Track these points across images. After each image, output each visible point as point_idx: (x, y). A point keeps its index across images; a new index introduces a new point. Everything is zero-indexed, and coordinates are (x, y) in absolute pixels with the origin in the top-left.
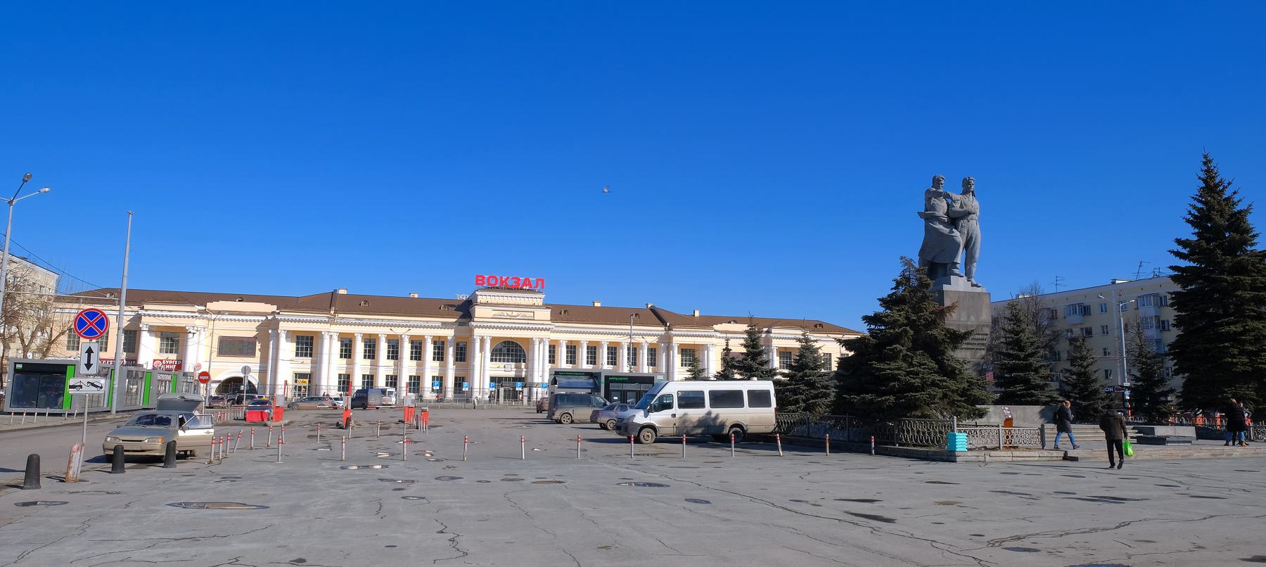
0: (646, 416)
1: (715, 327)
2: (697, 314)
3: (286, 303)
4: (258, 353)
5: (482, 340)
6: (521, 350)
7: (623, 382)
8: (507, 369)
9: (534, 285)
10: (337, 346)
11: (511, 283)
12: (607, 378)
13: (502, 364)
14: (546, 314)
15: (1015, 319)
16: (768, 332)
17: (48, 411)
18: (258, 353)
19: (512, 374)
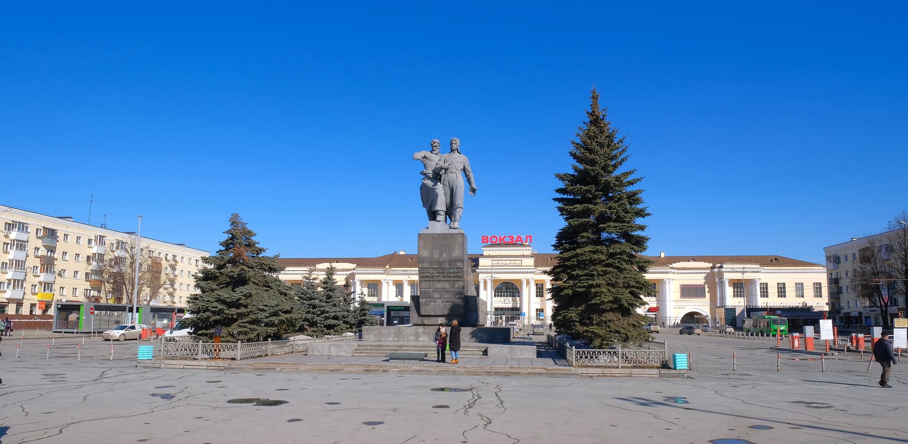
0: (171, 333)
1: (674, 265)
2: (663, 255)
3: (362, 263)
4: (708, 295)
5: (485, 282)
6: (516, 289)
7: (401, 310)
8: (506, 302)
9: (524, 240)
10: (533, 288)
11: (507, 240)
12: (388, 307)
13: (502, 299)
14: (531, 261)
15: (872, 243)
16: (721, 267)
17: (63, 330)
18: (708, 295)
19: (510, 305)
